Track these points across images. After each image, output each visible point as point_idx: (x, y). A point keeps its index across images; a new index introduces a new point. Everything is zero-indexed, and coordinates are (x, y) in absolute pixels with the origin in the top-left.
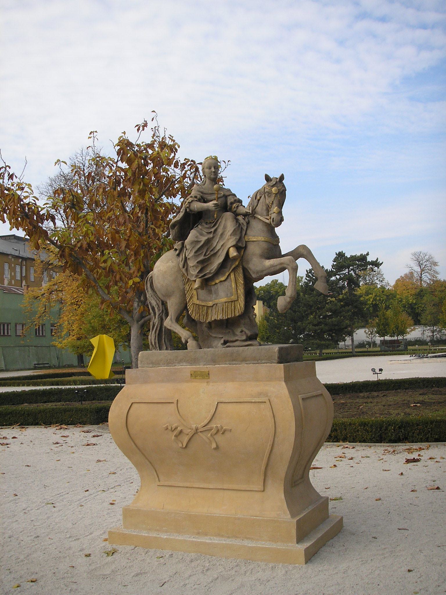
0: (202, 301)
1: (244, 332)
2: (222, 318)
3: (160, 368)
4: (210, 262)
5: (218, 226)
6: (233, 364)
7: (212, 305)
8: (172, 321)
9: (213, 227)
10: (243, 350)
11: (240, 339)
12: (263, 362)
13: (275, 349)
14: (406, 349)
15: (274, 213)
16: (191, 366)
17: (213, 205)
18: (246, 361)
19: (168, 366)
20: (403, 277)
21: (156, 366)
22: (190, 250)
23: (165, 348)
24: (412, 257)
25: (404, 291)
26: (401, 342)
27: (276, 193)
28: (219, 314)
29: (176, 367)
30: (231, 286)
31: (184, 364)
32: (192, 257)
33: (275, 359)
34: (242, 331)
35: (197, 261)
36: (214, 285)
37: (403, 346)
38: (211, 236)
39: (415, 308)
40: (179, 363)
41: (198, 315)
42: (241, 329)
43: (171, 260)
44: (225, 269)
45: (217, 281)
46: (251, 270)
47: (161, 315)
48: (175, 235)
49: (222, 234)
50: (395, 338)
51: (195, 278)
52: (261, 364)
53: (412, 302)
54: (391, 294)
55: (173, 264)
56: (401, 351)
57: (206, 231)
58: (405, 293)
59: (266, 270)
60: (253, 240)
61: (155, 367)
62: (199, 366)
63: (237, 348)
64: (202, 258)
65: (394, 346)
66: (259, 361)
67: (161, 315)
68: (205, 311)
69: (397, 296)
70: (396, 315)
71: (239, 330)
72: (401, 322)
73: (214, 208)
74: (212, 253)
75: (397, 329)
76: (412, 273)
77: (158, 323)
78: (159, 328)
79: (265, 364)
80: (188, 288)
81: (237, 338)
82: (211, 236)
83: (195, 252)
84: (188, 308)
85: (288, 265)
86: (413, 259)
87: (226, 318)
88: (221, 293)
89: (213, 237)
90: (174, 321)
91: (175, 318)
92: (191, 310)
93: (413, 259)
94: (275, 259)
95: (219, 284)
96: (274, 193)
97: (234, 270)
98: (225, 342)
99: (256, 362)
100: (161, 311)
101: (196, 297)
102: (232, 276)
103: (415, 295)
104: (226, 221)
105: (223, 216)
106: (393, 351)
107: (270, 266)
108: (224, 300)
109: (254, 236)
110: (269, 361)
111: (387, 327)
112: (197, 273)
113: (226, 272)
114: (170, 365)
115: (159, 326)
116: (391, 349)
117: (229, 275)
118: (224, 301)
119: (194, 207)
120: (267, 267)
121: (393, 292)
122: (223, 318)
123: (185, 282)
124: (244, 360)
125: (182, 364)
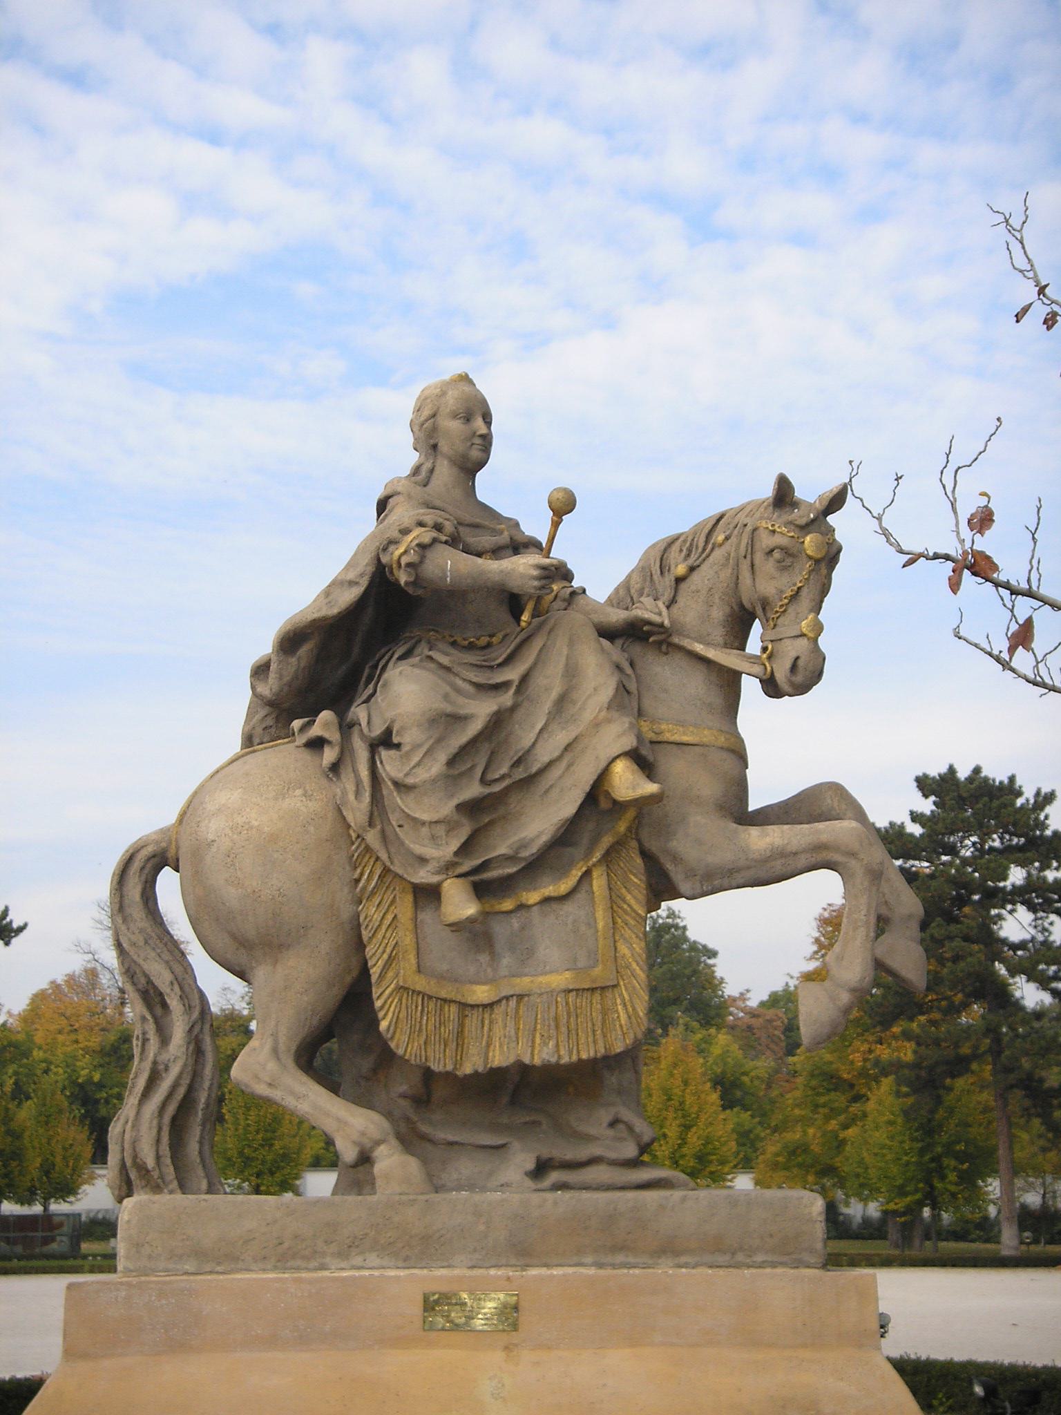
0: (441, 978)
1: (621, 1126)
2: (553, 1060)
3: (239, 1276)
4: (501, 811)
5: (535, 664)
6: (614, 1266)
7: (486, 1001)
8: (278, 1059)
9: (508, 661)
10: (662, 1207)
11: (613, 1155)
12: (759, 1258)
13: (812, 1204)
14: (75, 1253)
15: (803, 635)
16: (407, 1272)
17: (535, 573)
18: (676, 1253)
19: (284, 1270)
20: (60, 985)
21: (219, 1269)
22: (424, 749)
23: (204, 1185)
24: (97, 916)
25: (61, 1038)
26: (61, 1225)
27: (819, 556)
28: (538, 1041)
29: (326, 1273)
30: (592, 924)
31: (373, 1259)
32: (434, 781)
33: (811, 1251)
34: (613, 1124)
35: (455, 802)
36: (511, 912)
37: (64, 1239)
38: (507, 699)
39: (97, 1101)
40: (342, 1255)
41: (422, 1042)
42: (613, 1110)
43: (300, 785)
44: (570, 850)
45: (533, 897)
46: (676, 859)
47: (197, 1029)
48: (289, 684)
49: (562, 702)
50: (37, 1209)
51: (438, 873)
52: (749, 1267)
53: (89, 1080)
54: (11, 1044)
55: (310, 804)
56: (63, 1257)
57: (475, 680)
58: (64, 1045)
59: (749, 868)
60: (676, 738)
61: (211, 1272)
62: (444, 1272)
63: (631, 1195)
64: (473, 790)
65: (33, 1237)
66: (740, 1257)
67: (197, 1029)
68: (452, 1026)
69: (35, 1053)
70: (47, 1123)
71: (605, 1116)
72: (65, 1149)
73: (536, 583)
74: (520, 774)
75: (47, 1173)
76: (92, 974)
77: (185, 1065)
78: (181, 1091)
79: (768, 1270)
80: (377, 917)
81: (595, 1150)
82: (507, 699)
83: (451, 763)
84: (378, 1004)
85: (853, 854)
86: (101, 923)
87: (575, 1058)
88: (550, 950)
89: (513, 709)
90: (290, 1063)
91: (294, 1048)
92: (390, 1014)
93: (101, 923)
94: (786, 827)
95: (535, 908)
96: (810, 558)
97: (608, 858)
98: (541, 1169)
99: (721, 1259)
100: (196, 1014)
101: (413, 961)
102: (599, 882)
103: (102, 1052)
104: (571, 643)
105: (555, 625)
106: (30, 1257)
107: (768, 854)
108: (559, 980)
109: (681, 723)
110: (785, 1259)
111: (14, 1164)
112: (456, 854)
113: (571, 864)
114: (299, 1263)
115: (186, 1081)
116: (19, 1249)
117: (587, 874)
118: (563, 987)
119: (444, 571)
120: (756, 856)
121: (21, 1037)
122: (559, 1057)
123: (364, 888)
124: (669, 1249)
125: (358, 1261)
